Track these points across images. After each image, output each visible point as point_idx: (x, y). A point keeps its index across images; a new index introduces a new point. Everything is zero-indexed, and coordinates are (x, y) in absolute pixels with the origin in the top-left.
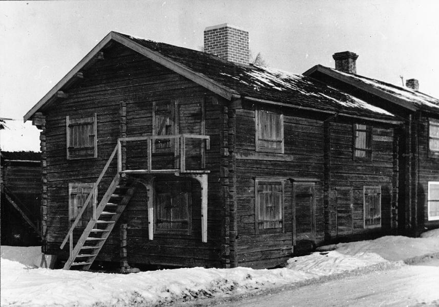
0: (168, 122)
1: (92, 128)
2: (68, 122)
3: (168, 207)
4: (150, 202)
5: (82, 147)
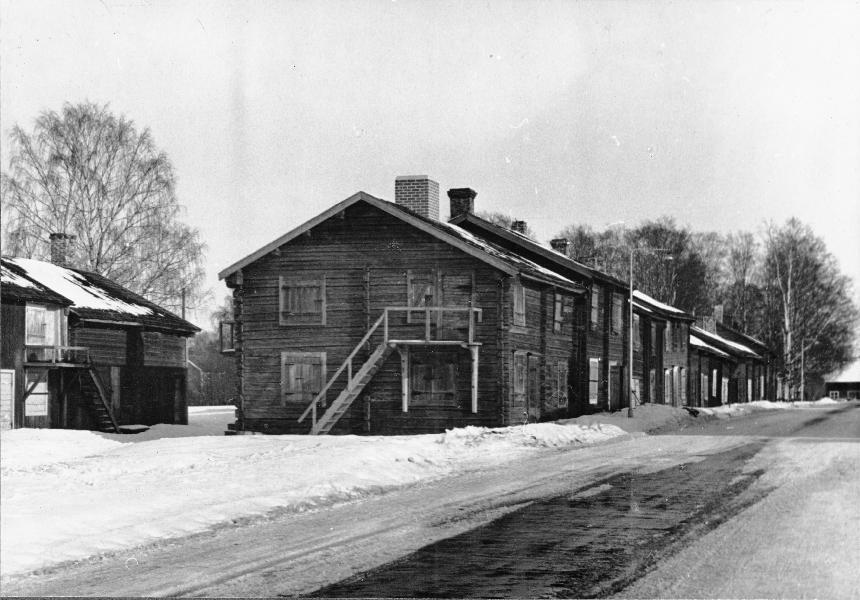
0: (428, 291)
1: (319, 293)
2: (282, 283)
3: (428, 379)
4: (405, 374)
5: (304, 311)
